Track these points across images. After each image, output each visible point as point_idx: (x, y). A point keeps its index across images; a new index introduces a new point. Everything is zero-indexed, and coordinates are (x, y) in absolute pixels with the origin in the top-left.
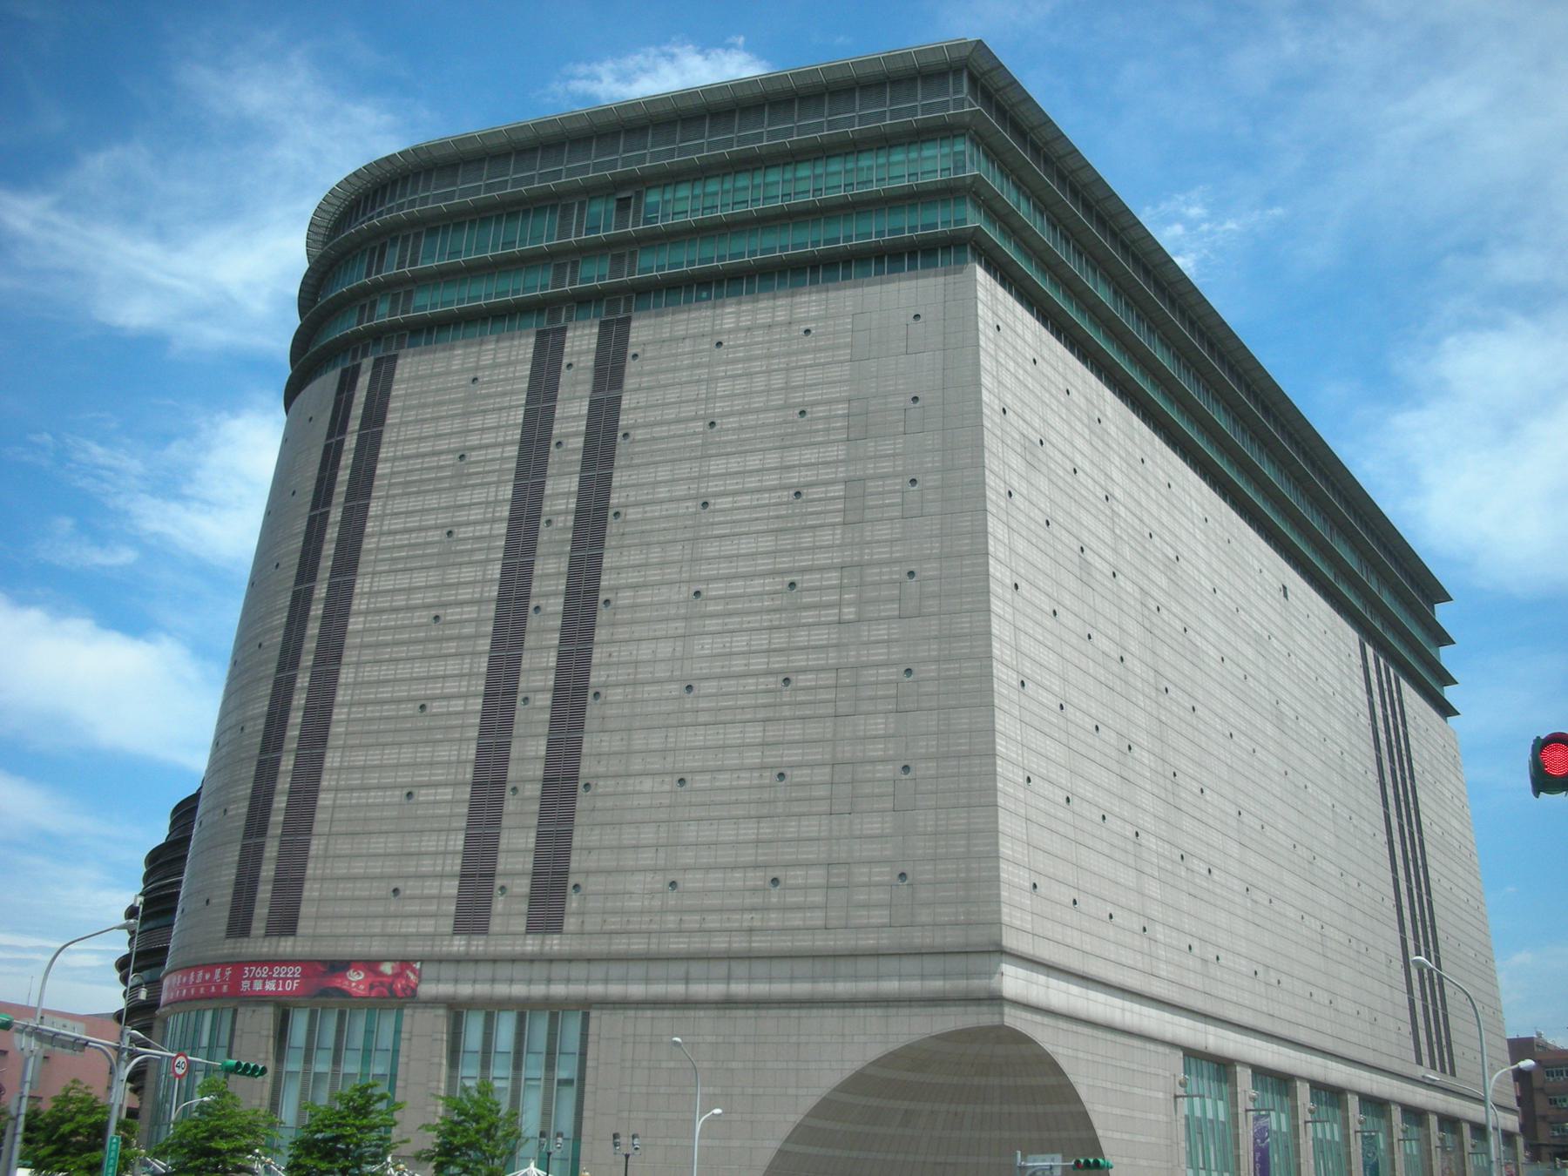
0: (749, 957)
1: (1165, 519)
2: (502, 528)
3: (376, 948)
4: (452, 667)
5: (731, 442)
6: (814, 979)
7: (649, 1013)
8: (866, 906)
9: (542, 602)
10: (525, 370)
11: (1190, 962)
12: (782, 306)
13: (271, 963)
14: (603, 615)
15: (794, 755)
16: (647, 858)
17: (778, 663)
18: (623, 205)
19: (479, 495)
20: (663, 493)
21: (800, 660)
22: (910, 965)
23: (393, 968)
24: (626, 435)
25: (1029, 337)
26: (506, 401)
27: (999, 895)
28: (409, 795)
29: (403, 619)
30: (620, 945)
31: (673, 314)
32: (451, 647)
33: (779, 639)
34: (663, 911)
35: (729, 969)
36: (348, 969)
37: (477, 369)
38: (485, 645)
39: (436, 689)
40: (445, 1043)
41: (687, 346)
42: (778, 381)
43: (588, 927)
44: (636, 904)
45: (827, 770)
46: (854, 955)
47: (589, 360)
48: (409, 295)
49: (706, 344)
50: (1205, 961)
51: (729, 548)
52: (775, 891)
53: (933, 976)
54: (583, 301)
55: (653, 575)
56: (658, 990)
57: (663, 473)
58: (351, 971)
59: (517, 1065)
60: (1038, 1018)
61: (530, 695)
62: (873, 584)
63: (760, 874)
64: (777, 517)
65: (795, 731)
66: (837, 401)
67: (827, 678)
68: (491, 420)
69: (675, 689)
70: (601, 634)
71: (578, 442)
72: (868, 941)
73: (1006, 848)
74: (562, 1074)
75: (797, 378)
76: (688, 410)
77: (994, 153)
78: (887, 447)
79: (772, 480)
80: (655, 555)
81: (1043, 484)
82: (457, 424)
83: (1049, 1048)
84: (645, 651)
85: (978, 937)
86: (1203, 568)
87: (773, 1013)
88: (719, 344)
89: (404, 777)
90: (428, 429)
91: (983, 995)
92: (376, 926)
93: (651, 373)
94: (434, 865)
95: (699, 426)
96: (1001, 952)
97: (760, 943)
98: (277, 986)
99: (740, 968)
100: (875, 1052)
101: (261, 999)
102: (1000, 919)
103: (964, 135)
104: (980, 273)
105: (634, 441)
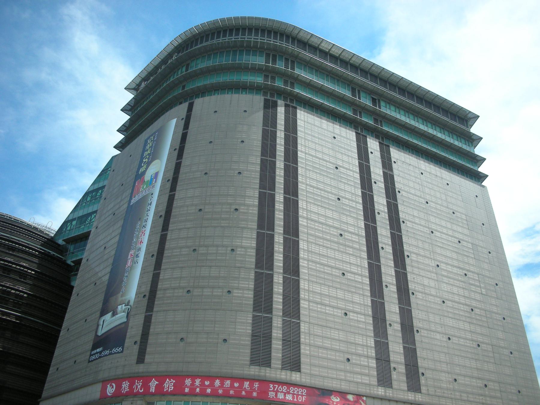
3: (344, 387)
23: (353, 398)
36: (331, 395)
58: (333, 396)
63: (450, 376)
98: (293, 398)
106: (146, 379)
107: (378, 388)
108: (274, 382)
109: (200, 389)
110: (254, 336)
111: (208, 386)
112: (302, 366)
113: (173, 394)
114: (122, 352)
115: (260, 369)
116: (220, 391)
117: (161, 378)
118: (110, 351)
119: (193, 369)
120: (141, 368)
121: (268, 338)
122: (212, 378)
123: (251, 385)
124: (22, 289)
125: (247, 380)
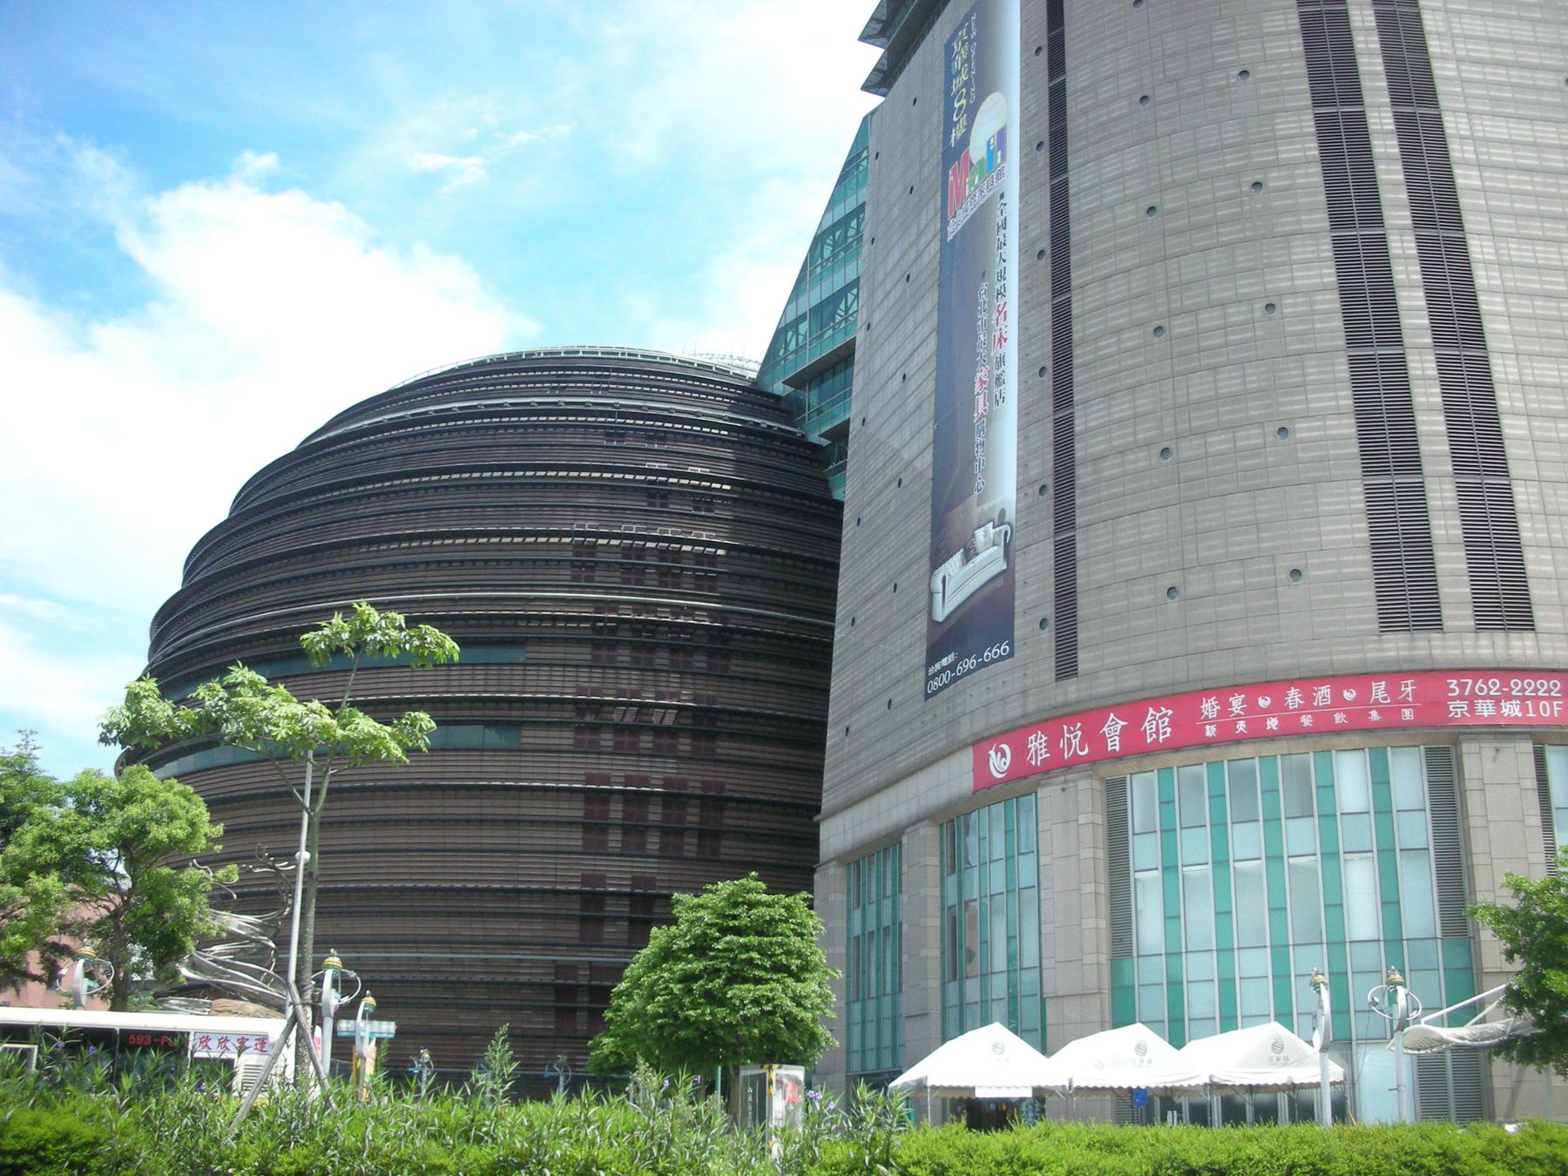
106: (1090, 717)
109: (1248, 722)
111: (1269, 711)
112: (1538, 613)
113: (1172, 747)
114: (1011, 654)
115: (1413, 640)
116: (1306, 721)
117: (1133, 708)
118: (976, 658)
119: (1219, 667)
120: (1072, 690)
121: (1422, 544)
122: (1275, 686)
123: (1393, 691)
124: (707, 536)
125: (1377, 676)
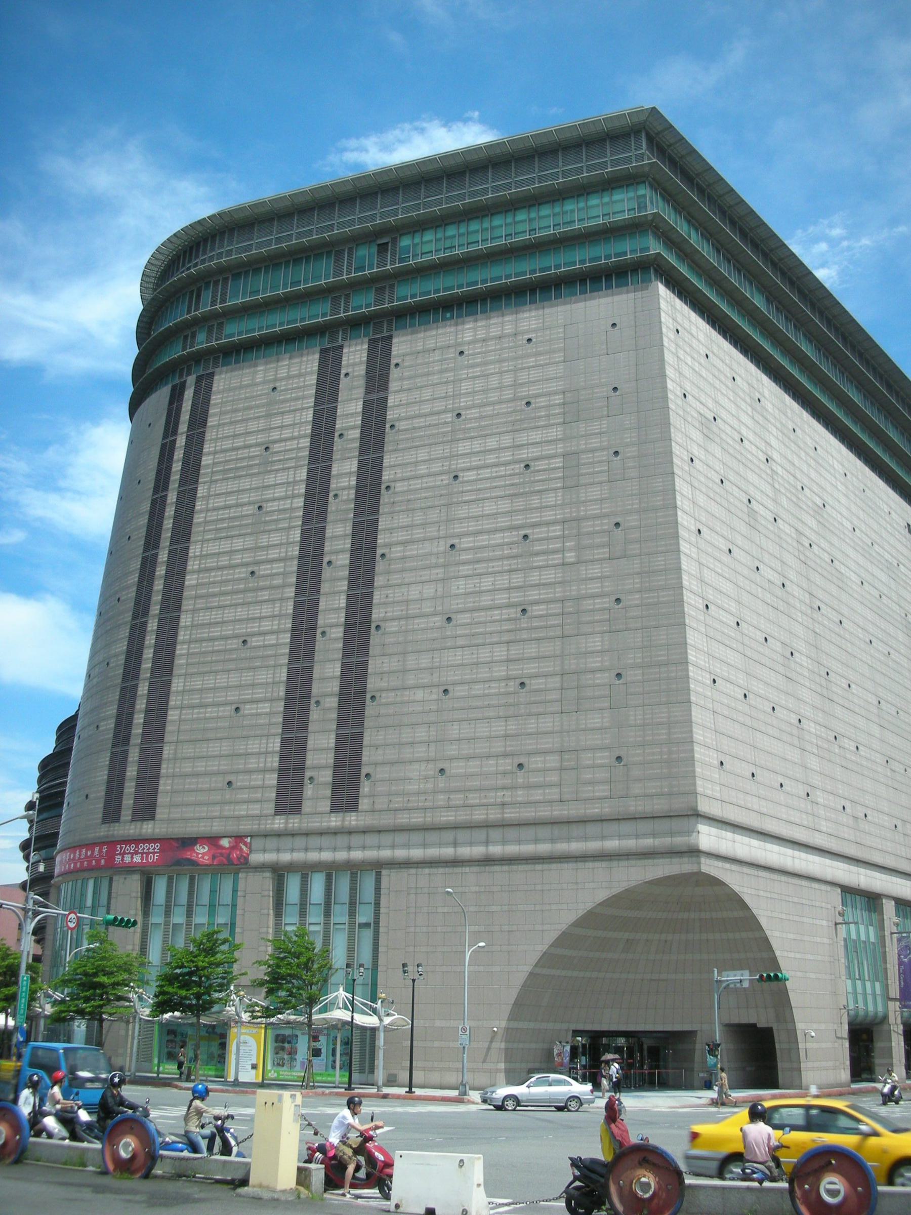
0: (502, 825)
1: (813, 475)
2: (300, 502)
3: (217, 828)
4: (266, 610)
5: (473, 428)
6: (553, 841)
7: (427, 871)
8: (591, 783)
9: (333, 558)
10: (313, 379)
11: (844, 818)
12: (509, 321)
13: (137, 841)
14: (380, 566)
15: (531, 668)
16: (421, 751)
17: (516, 597)
18: (383, 248)
19: (281, 478)
20: (423, 469)
21: (533, 595)
22: (626, 827)
23: (230, 842)
24: (392, 426)
25: (701, 337)
26: (299, 404)
27: (694, 771)
28: (237, 709)
29: (227, 575)
30: (403, 819)
31: (425, 331)
32: (265, 595)
33: (517, 579)
34: (435, 792)
35: (487, 834)
37: (276, 380)
38: (290, 592)
39: (254, 627)
40: (271, 899)
41: (437, 356)
42: (508, 379)
43: (378, 807)
44: (414, 787)
45: (558, 678)
46: (583, 821)
47: (361, 370)
48: (221, 326)
49: (452, 354)
50: (856, 818)
51: (475, 510)
52: (520, 774)
53: (645, 836)
54: (355, 325)
55: (418, 533)
56: (433, 852)
57: (423, 454)
59: (327, 913)
60: (727, 866)
61: (327, 629)
62: (588, 533)
63: (508, 761)
64: (512, 485)
65: (531, 650)
66: (555, 393)
67: (555, 608)
68: (288, 419)
69: (438, 621)
70: (379, 581)
71: (356, 434)
72: (594, 810)
73: (698, 734)
74: (361, 919)
75: (523, 377)
76: (439, 406)
77: (669, 196)
78: (595, 427)
79: (507, 456)
80: (419, 518)
81: (718, 452)
82: (262, 424)
83: (736, 888)
84: (414, 592)
85: (679, 804)
86: (845, 512)
87: (522, 867)
88: (462, 353)
89: (233, 696)
90: (240, 429)
91: (684, 849)
92: (216, 811)
93: (410, 378)
94: (258, 763)
95: (449, 417)
96: (697, 815)
97: (510, 814)
98: (142, 859)
99: (495, 834)
100: (602, 895)
101: (130, 869)
102: (695, 789)
103: (644, 182)
104: (662, 290)
105: (399, 431)
107: (273, 820)
108: (128, 842)
110: (110, 781)
